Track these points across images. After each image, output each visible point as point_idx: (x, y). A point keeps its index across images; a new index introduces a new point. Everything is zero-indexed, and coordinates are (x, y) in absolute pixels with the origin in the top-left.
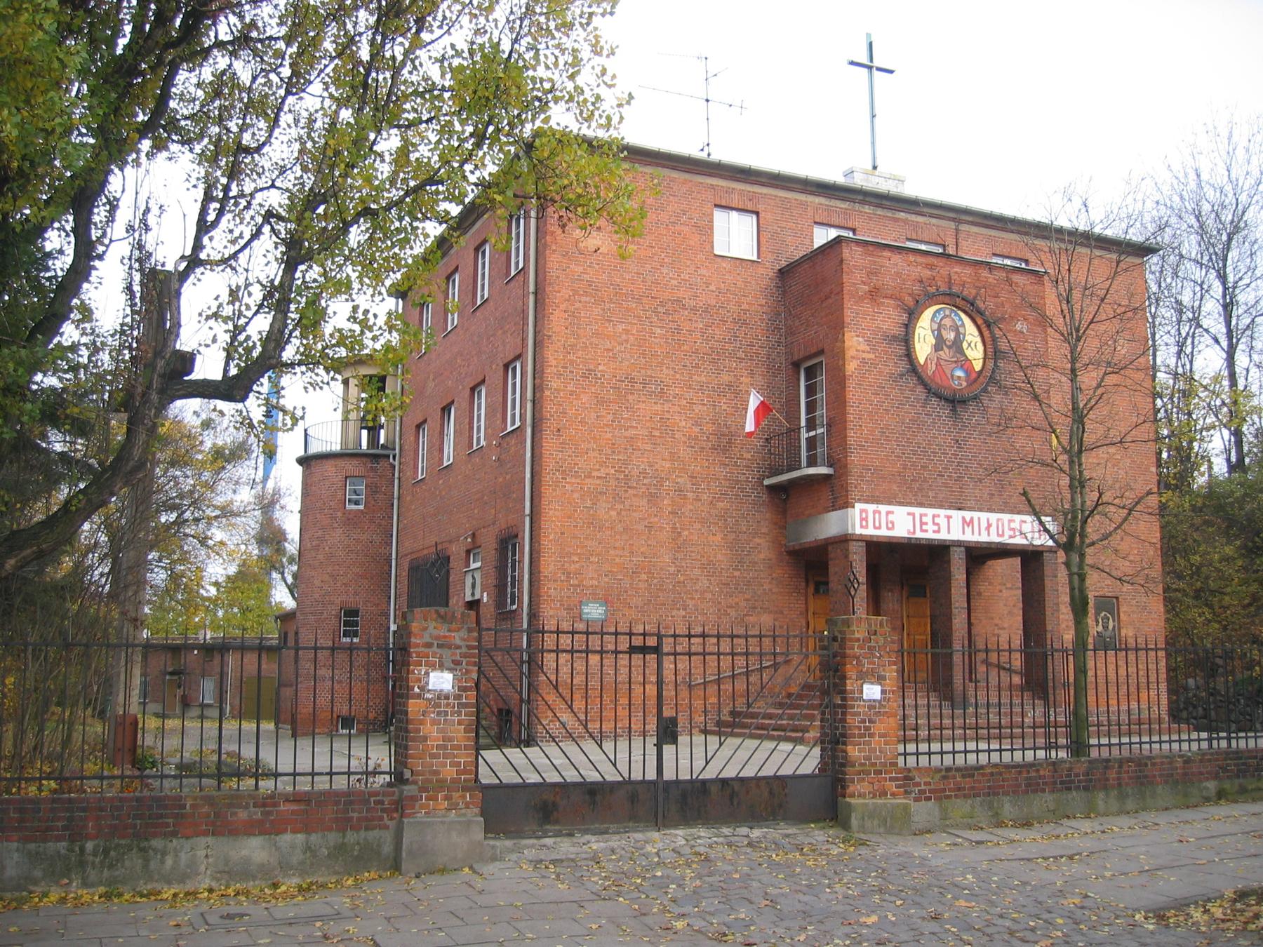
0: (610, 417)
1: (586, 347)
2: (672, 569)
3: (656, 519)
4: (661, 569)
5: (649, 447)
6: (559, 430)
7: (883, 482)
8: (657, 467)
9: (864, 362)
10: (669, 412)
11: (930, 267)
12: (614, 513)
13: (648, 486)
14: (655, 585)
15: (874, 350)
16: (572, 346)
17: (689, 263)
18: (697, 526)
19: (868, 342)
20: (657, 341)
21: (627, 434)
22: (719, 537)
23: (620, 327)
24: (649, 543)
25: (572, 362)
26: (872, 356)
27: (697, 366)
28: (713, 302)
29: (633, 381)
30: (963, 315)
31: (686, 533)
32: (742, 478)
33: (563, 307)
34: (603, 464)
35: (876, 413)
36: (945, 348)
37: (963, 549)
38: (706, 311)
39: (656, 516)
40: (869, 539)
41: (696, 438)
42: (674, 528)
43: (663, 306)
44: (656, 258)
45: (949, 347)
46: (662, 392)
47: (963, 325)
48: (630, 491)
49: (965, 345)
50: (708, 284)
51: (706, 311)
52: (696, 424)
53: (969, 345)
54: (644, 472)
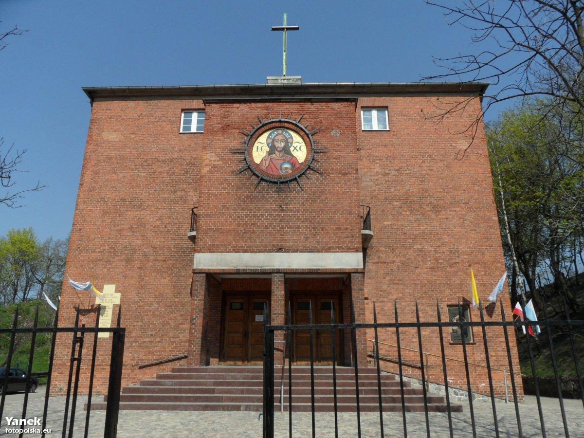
0: (109, 221)
1: (101, 187)
2: (136, 299)
4: (130, 299)
6: (80, 229)
7: (222, 235)
9: (214, 167)
11: (267, 108)
12: (105, 270)
14: (125, 308)
15: (222, 159)
16: (93, 188)
19: (218, 155)
20: (140, 179)
21: (118, 228)
22: (166, 280)
23: (121, 175)
24: (124, 285)
25: (92, 195)
26: (220, 163)
28: (175, 156)
29: (125, 201)
30: (292, 133)
33: (91, 169)
34: (102, 245)
35: (220, 195)
36: (276, 152)
37: (204, 275)
38: (171, 161)
40: (207, 271)
41: (158, 227)
45: (280, 152)
47: (291, 137)
48: (116, 258)
49: (292, 149)
51: (171, 161)
52: (159, 219)
53: (295, 148)
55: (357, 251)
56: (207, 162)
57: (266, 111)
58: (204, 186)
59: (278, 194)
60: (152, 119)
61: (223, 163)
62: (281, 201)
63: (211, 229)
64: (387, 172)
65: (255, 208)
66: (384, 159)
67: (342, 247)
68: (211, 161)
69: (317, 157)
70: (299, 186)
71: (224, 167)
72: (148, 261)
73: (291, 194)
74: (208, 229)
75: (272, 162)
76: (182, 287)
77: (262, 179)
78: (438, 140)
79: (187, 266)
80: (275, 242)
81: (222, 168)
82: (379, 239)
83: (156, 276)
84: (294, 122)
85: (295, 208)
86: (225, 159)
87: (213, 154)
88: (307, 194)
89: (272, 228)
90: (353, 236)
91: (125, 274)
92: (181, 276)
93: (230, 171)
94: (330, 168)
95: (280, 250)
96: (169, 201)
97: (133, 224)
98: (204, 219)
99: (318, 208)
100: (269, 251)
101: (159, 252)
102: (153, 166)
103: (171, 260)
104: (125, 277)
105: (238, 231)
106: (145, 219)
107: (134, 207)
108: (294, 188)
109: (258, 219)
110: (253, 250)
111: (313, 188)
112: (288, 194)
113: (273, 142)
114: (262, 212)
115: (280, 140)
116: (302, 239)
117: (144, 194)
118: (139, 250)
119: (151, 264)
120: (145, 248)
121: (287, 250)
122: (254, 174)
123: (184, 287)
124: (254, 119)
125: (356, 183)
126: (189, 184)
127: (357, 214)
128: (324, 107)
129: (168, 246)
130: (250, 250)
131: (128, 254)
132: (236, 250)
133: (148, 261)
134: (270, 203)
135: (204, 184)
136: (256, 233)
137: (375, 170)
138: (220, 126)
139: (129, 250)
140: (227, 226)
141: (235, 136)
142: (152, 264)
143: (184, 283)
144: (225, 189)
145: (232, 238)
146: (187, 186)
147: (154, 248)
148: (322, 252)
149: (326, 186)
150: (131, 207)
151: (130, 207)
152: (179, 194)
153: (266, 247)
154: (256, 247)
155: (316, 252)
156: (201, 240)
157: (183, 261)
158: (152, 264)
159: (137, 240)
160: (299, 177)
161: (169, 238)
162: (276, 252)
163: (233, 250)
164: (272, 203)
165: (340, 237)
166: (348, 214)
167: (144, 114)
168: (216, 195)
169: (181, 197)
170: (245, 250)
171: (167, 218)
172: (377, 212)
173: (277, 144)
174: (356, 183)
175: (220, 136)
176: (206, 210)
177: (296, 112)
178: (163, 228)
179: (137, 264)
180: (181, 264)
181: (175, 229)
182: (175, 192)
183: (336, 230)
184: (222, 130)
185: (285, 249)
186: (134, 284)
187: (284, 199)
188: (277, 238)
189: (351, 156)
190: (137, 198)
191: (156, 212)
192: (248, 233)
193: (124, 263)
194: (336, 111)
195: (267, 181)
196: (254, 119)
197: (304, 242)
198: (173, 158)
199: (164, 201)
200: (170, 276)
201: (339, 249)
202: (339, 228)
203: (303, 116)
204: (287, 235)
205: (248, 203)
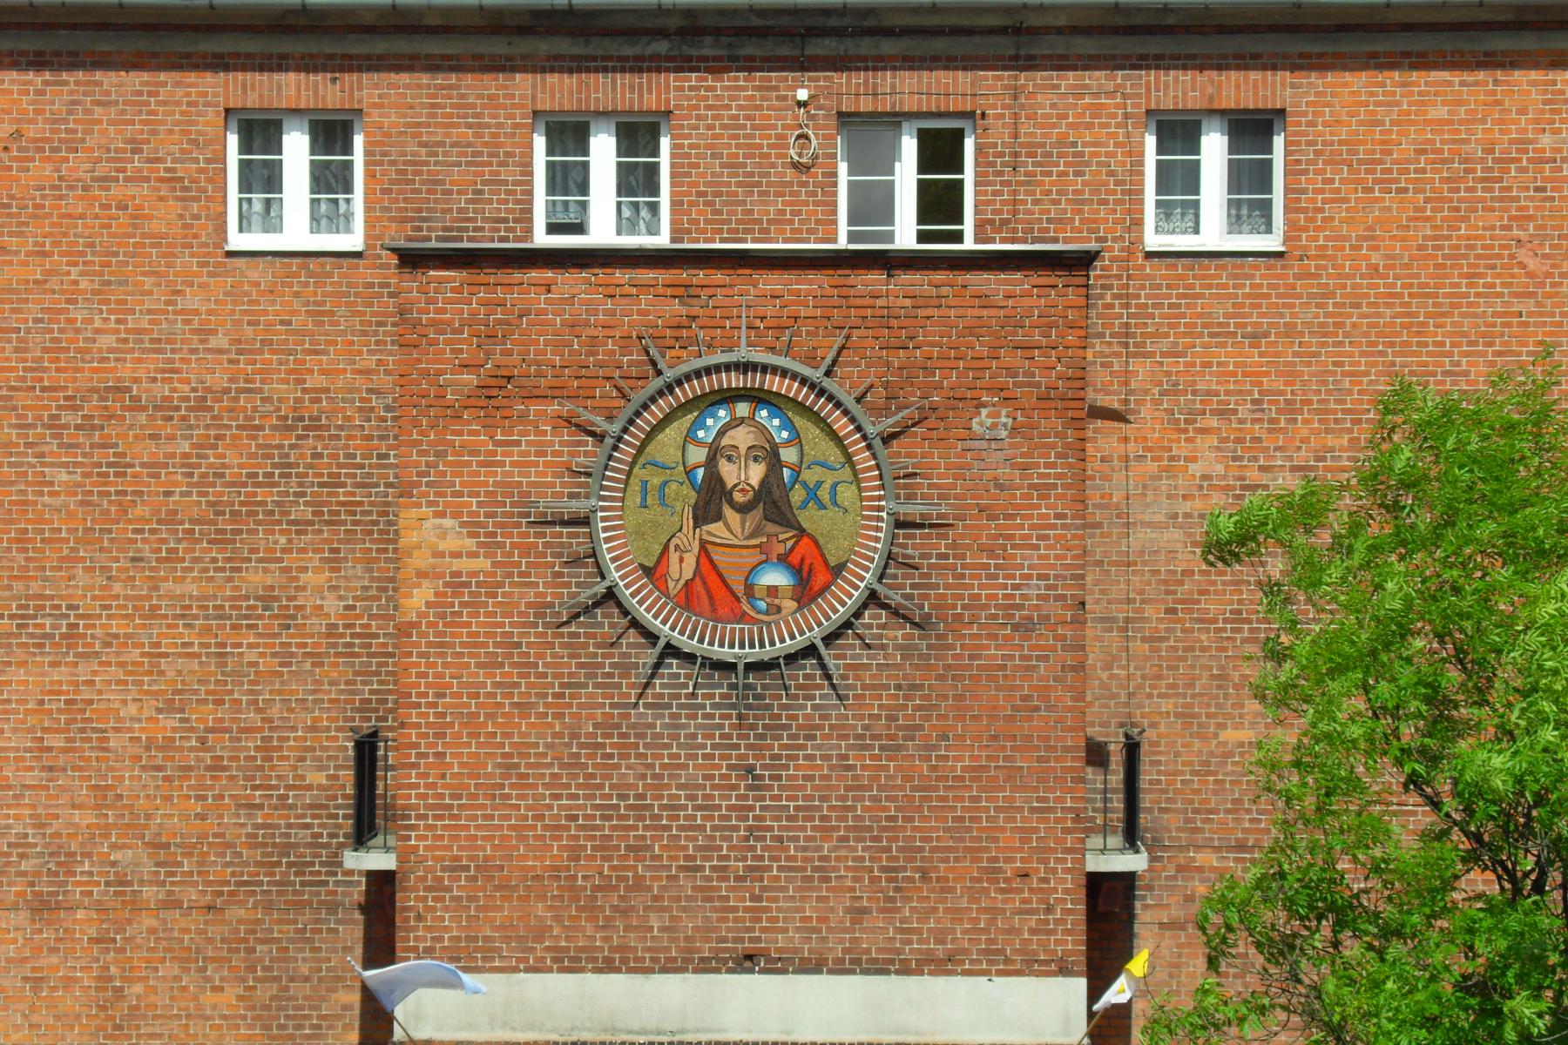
3: (55, 960)
5: (31, 778)
8: (56, 825)
9: (457, 583)
10: (92, 683)
11: (686, 293)
13: (32, 878)
15: (490, 547)
17: (148, 281)
18: (169, 969)
19: (473, 528)
20: (56, 501)
22: (231, 993)
24: (35, 1019)
26: (484, 563)
27: (172, 557)
28: (219, 380)
31: (138, 988)
32: (304, 836)
35: (489, 716)
36: (728, 512)
38: (201, 406)
39: (53, 950)
41: (168, 746)
42: (104, 978)
43: (76, 408)
44: (54, 283)
45: (743, 509)
46: (72, 636)
50: (205, 333)
51: (201, 406)
54: (21, 843)
55: (1064, 970)
56: (420, 561)
57: (677, 307)
58: (419, 675)
59: (740, 717)
60: (77, 165)
61: (495, 564)
62: (749, 747)
63: (456, 868)
64: (1253, 476)
65: (644, 777)
66: (1244, 411)
67: (1002, 951)
68: (441, 555)
69: (911, 548)
70: (828, 677)
71: (501, 585)
72: (136, 906)
73: (795, 718)
74: (443, 869)
75: (711, 561)
76: (301, 1027)
77: (671, 650)
78: (1529, 305)
79: (320, 931)
80: (728, 930)
81: (492, 588)
82: (1195, 811)
83: (177, 978)
84: (806, 371)
85: (811, 778)
86: (501, 545)
87: (448, 522)
88: (862, 717)
89: (713, 868)
90: (1049, 910)
91: (34, 969)
92: (292, 979)
93: (529, 605)
94: (962, 597)
95: (747, 961)
96: (207, 617)
97: (45, 730)
98: (428, 827)
99: (910, 779)
100: (705, 966)
101: (181, 864)
102: (112, 431)
103: (242, 903)
104: (37, 982)
105: (574, 878)
106: (102, 706)
107: (42, 646)
108: (808, 688)
109: (655, 828)
110: (637, 959)
111: (887, 687)
112: (779, 717)
113: (711, 463)
114: (671, 797)
115: (743, 451)
116: (839, 908)
117: (82, 579)
118: (89, 855)
119: (148, 921)
120: (113, 847)
121: (777, 964)
122: (635, 624)
123: (313, 1027)
124: (625, 349)
125: (1073, 668)
126: (301, 525)
127: (1071, 810)
128: (945, 290)
129: (223, 835)
130: (624, 961)
131: (38, 874)
132: (570, 962)
133: (136, 906)
134: (705, 756)
135: (418, 665)
136: (650, 889)
137: (1196, 469)
138: (469, 378)
139: (41, 854)
140: (524, 857)
141: (544, 433)
142: (154, 923)
143: (311, 1008)
144: (508, 687)
145: (551, 908)
146: (290, 541)
147: (158, 846)
148: (921, 973)
149: (942, 678)
150: (26, 645)
151: (20, 645)
152: (255, 578)
153: (691, 950)
154: (649, 949)
155: (898, 972)
156: (419, 918)
157: (300, 906)
158: (154, 923)
159: (74, 807)
160: (829, 639)
161: (221, 797)
162: (730, 971)
163: (555, 960)
164: (711, 757)
165: (993, 911)
166: (1033, 810)
167: (31, 131)
168: (471, 715)
169: (267, 599)
170: (605, 959)
171: (205, 701)
172: (1191, 685)
173: (729, 472)
174: (1073, 668)
175: (471, 433)
176: (433, 786)
177: (819, 312)
178: (191, 749)
179: (83, 922)
180: (288, 922)
181: (248, 758)
182: (233, 569)
183: (979, 880)
184: (483, 402)
185: (769, 960)
186: (78, 1017)
187: (762, 737)
188: (734, 909)
189: (1058, 538)
190: (52, 598)
191: (150, 673)
192: (616, 888)
193: (23, 917)
194: (993, 312)
195: (690, 658)
196: (625, 349)
197: (846, 931)
198: (208, 390)
199: (183, 616)
200: (244, 980)
201: (990, 962)
202: (992, 873)
203: (848, 337)
204: (775, 899)
205: (611, 756)
